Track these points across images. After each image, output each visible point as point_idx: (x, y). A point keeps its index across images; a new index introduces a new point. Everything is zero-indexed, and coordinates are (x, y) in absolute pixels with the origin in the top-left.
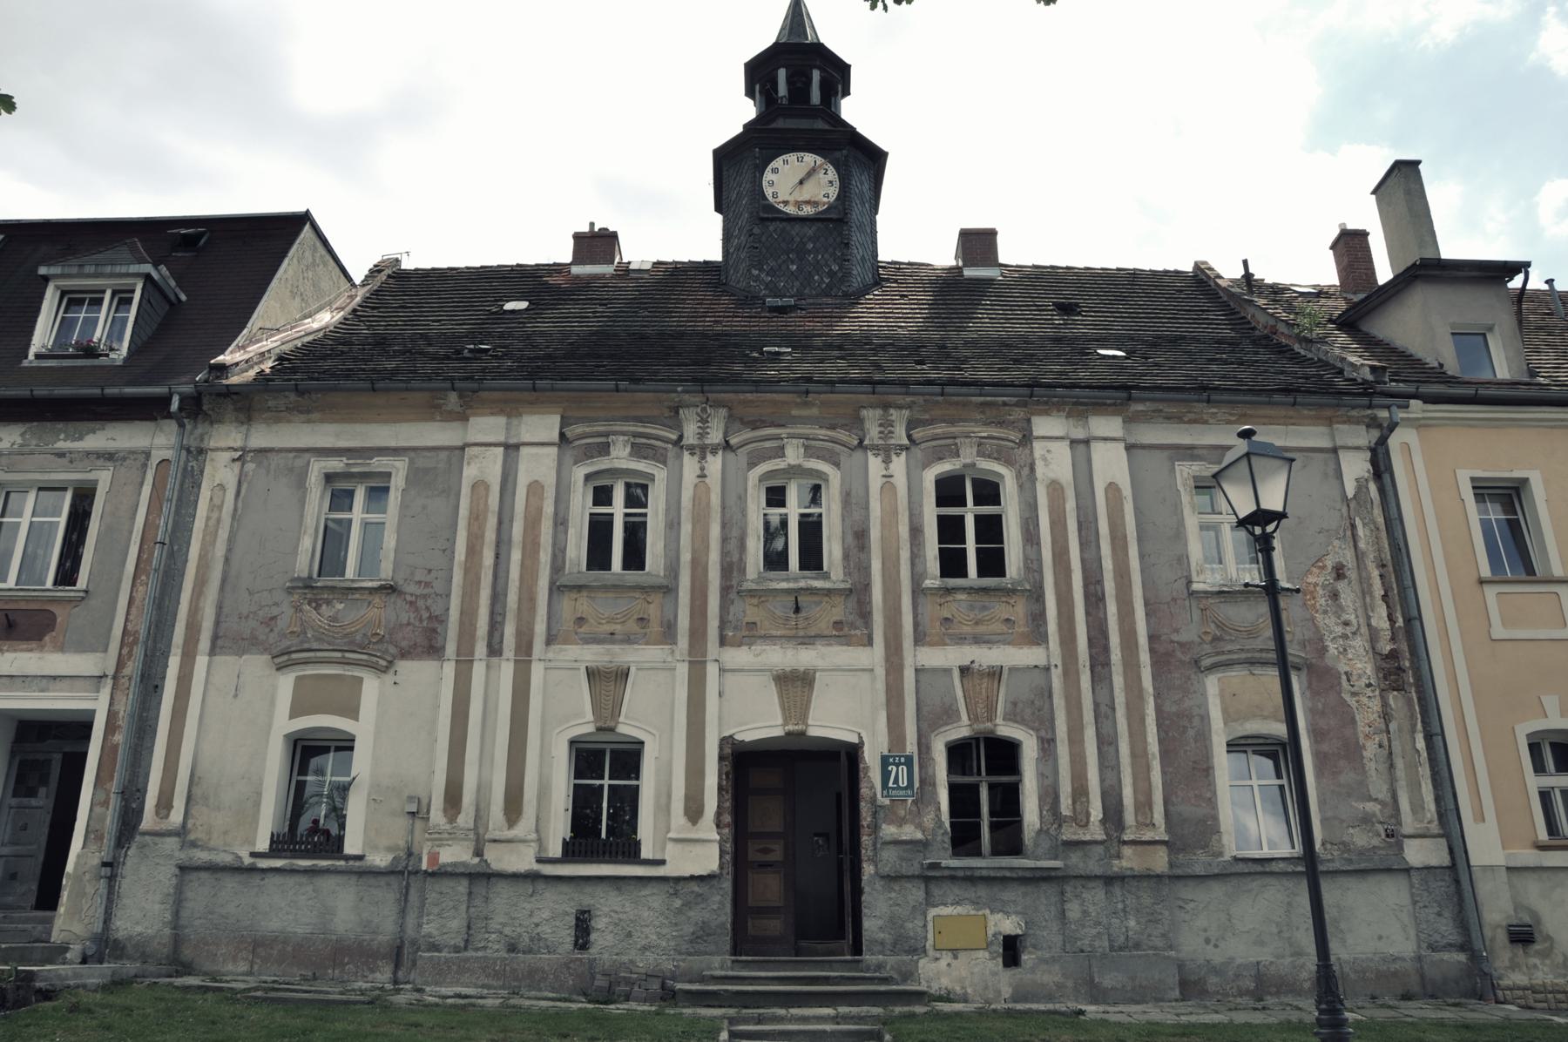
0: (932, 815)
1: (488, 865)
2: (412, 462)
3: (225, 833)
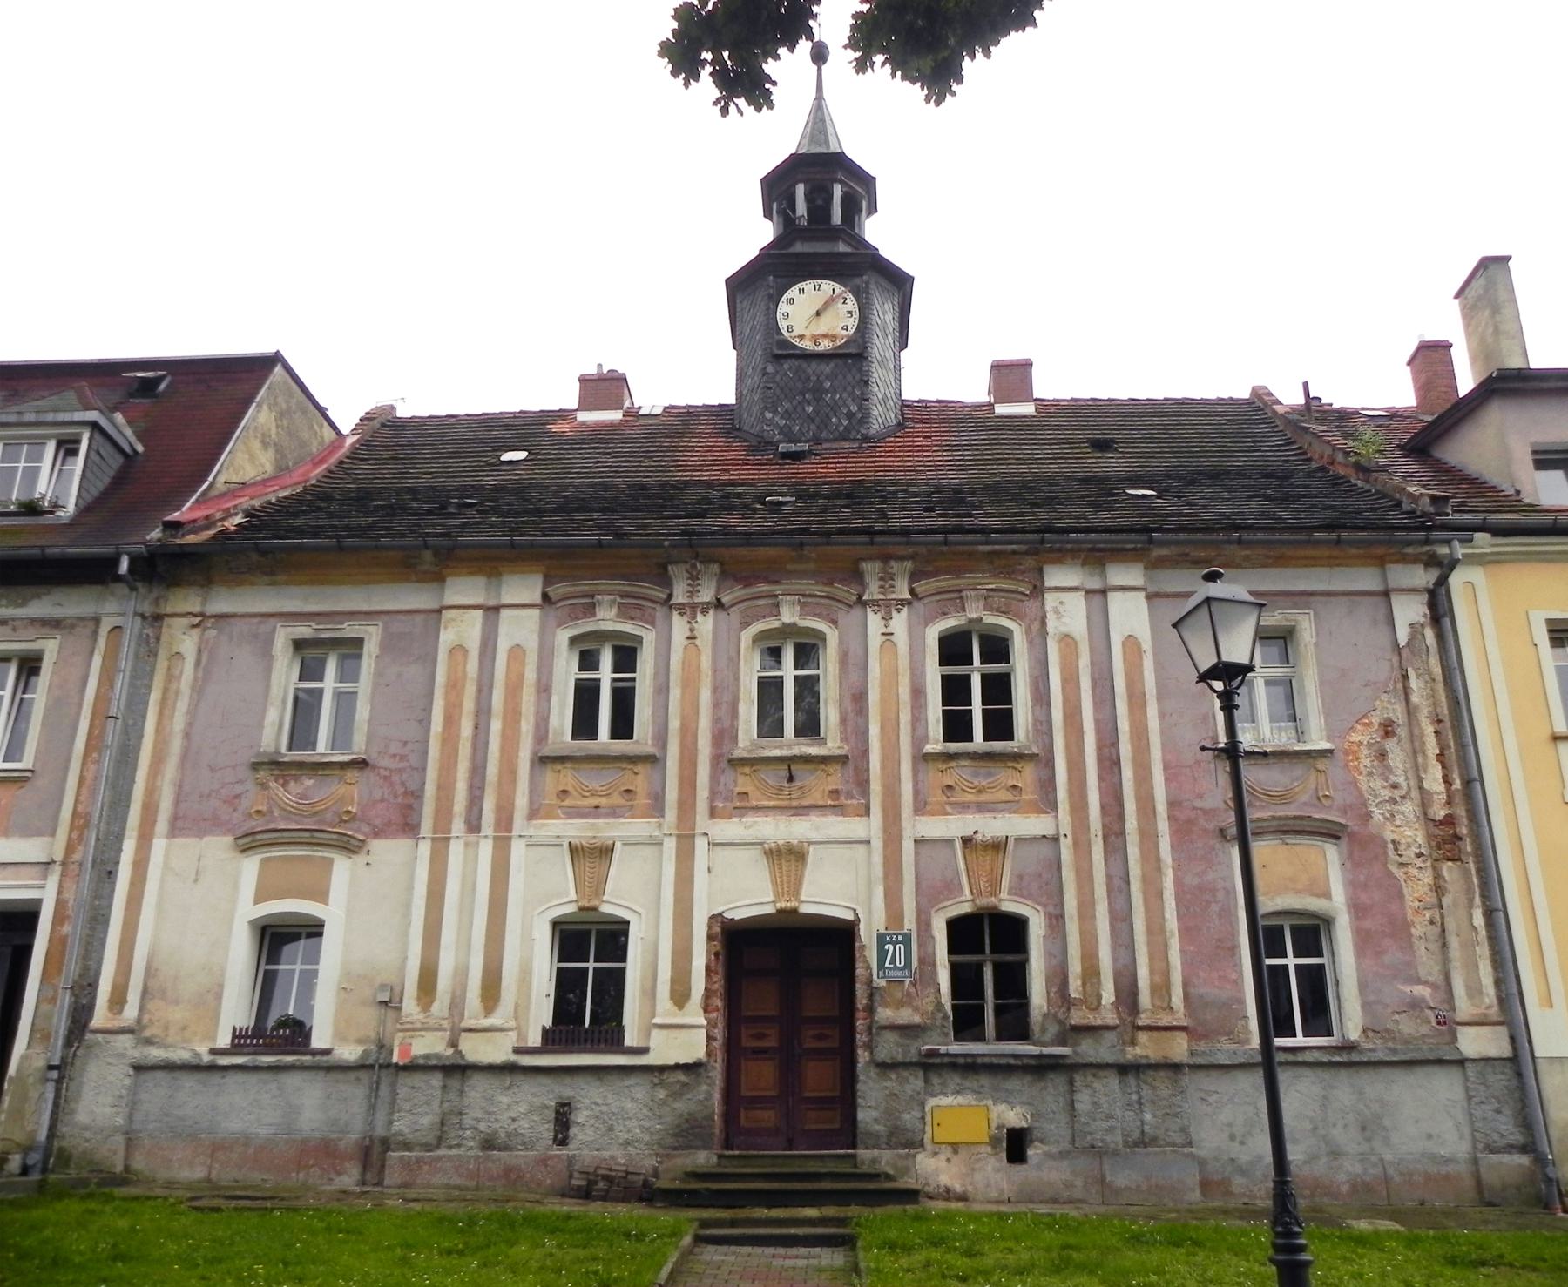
0: (932, 998)
1: (463, 1057)
2: (385, 629)
3: (184, 1028)
